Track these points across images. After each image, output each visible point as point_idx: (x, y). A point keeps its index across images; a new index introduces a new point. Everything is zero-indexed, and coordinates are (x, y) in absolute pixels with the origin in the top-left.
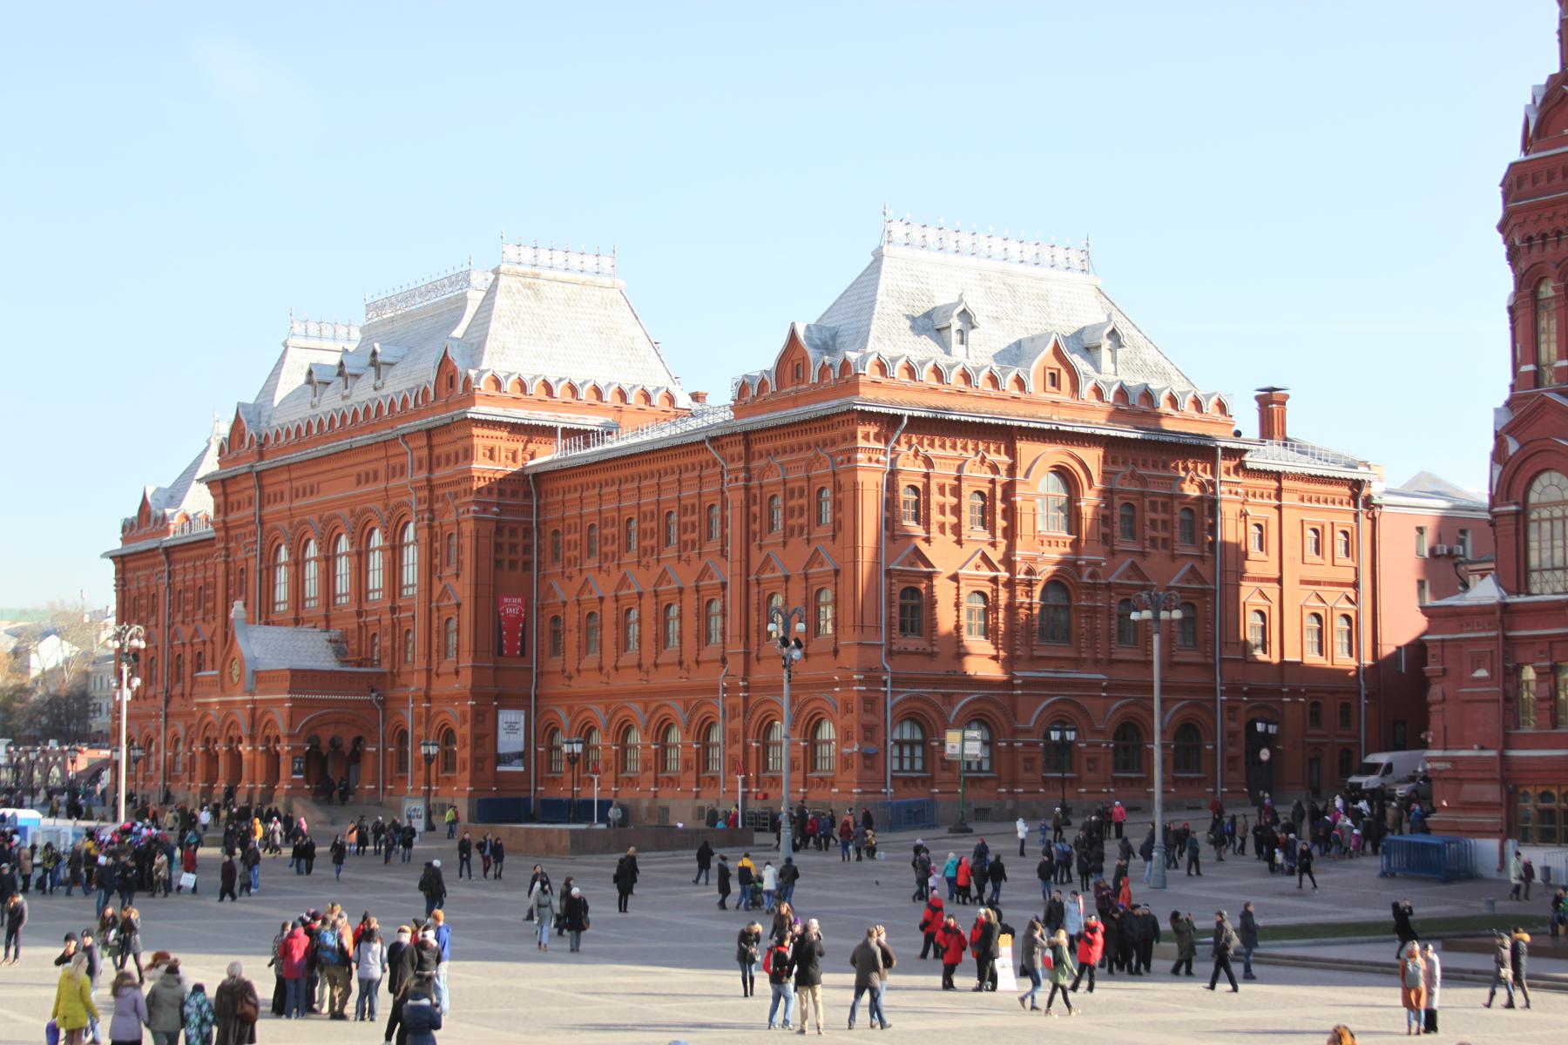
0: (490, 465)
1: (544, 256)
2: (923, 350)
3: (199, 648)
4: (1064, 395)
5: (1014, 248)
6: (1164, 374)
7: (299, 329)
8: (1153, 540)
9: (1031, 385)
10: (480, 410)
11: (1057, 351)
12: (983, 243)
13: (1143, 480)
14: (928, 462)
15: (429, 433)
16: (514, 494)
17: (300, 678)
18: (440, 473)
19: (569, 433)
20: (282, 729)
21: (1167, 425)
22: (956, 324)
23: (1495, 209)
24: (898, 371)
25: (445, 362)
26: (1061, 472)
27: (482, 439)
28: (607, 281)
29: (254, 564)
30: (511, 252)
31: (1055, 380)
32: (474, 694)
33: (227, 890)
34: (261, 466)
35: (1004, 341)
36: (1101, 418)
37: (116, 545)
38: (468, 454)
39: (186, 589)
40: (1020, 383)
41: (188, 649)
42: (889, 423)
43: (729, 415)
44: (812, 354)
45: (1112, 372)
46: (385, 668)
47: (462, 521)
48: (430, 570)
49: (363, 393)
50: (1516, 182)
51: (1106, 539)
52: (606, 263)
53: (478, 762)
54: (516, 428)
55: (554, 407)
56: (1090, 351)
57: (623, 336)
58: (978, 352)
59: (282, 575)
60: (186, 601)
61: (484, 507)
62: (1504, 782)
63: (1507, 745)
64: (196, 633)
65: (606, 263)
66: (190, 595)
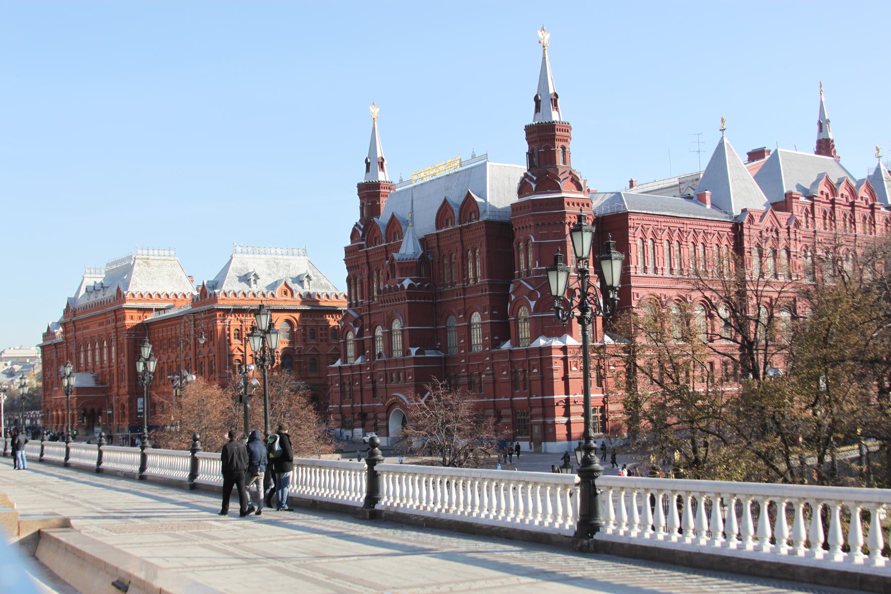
0: (131, 322)
1: (151, 252)
2: (244, 287)
3: (170, 364)
4: (289, 298)
5: (279, 251)
6: (328, 287)
7: (88, 271)
8: (322, 340)
9: (277, 295)
10: (128, 304)
11: (286, 284)
12: (268, 250)
13: (317, 321)
14: (242, 322)
15: (115, 311)
16: (140, 330)
17: (79, 390)
18: (119, 324)
19: (157, 310)
20: (75, 406)
21: (322, 304)
22: (253, 278)
23: (343, 256)
24: (231, 295)
25: (118, 289)
26: (288, 321)
27: (128, 314)
28: (172, 258)
29: (74, 351)
30: (139, 252)
31: (286, 293)
32: (129, 394)
33: (232, 487)
34: (74, 319)
35: (270, 281)
36: (298, 303)
37: (41, 342)
38: (124, 319)
39: (164, 339)
40: (273, 295)
41: (206, 359)
42: (227, 311)
43: (189, 308)
44: (208, 290)
45: (308, 288)
46: (108, 385)
47: (124, 338)
48: (117, 354)
49: (100, 296)
50: (348, 250)
51: (304, 340)
52: (172, 252)
53: (131, 415)
54: (139, 309)
55: (153, 301)
56: (301, 283)
57: (162, 283)
58: (259, 287)
59: (82, 355)
60: (164, 344)
61: (130, 335)
62: (341, 413)
63: (513, 396)
64: (169, 358)
65: (172, 252)
66: (165, 342)
